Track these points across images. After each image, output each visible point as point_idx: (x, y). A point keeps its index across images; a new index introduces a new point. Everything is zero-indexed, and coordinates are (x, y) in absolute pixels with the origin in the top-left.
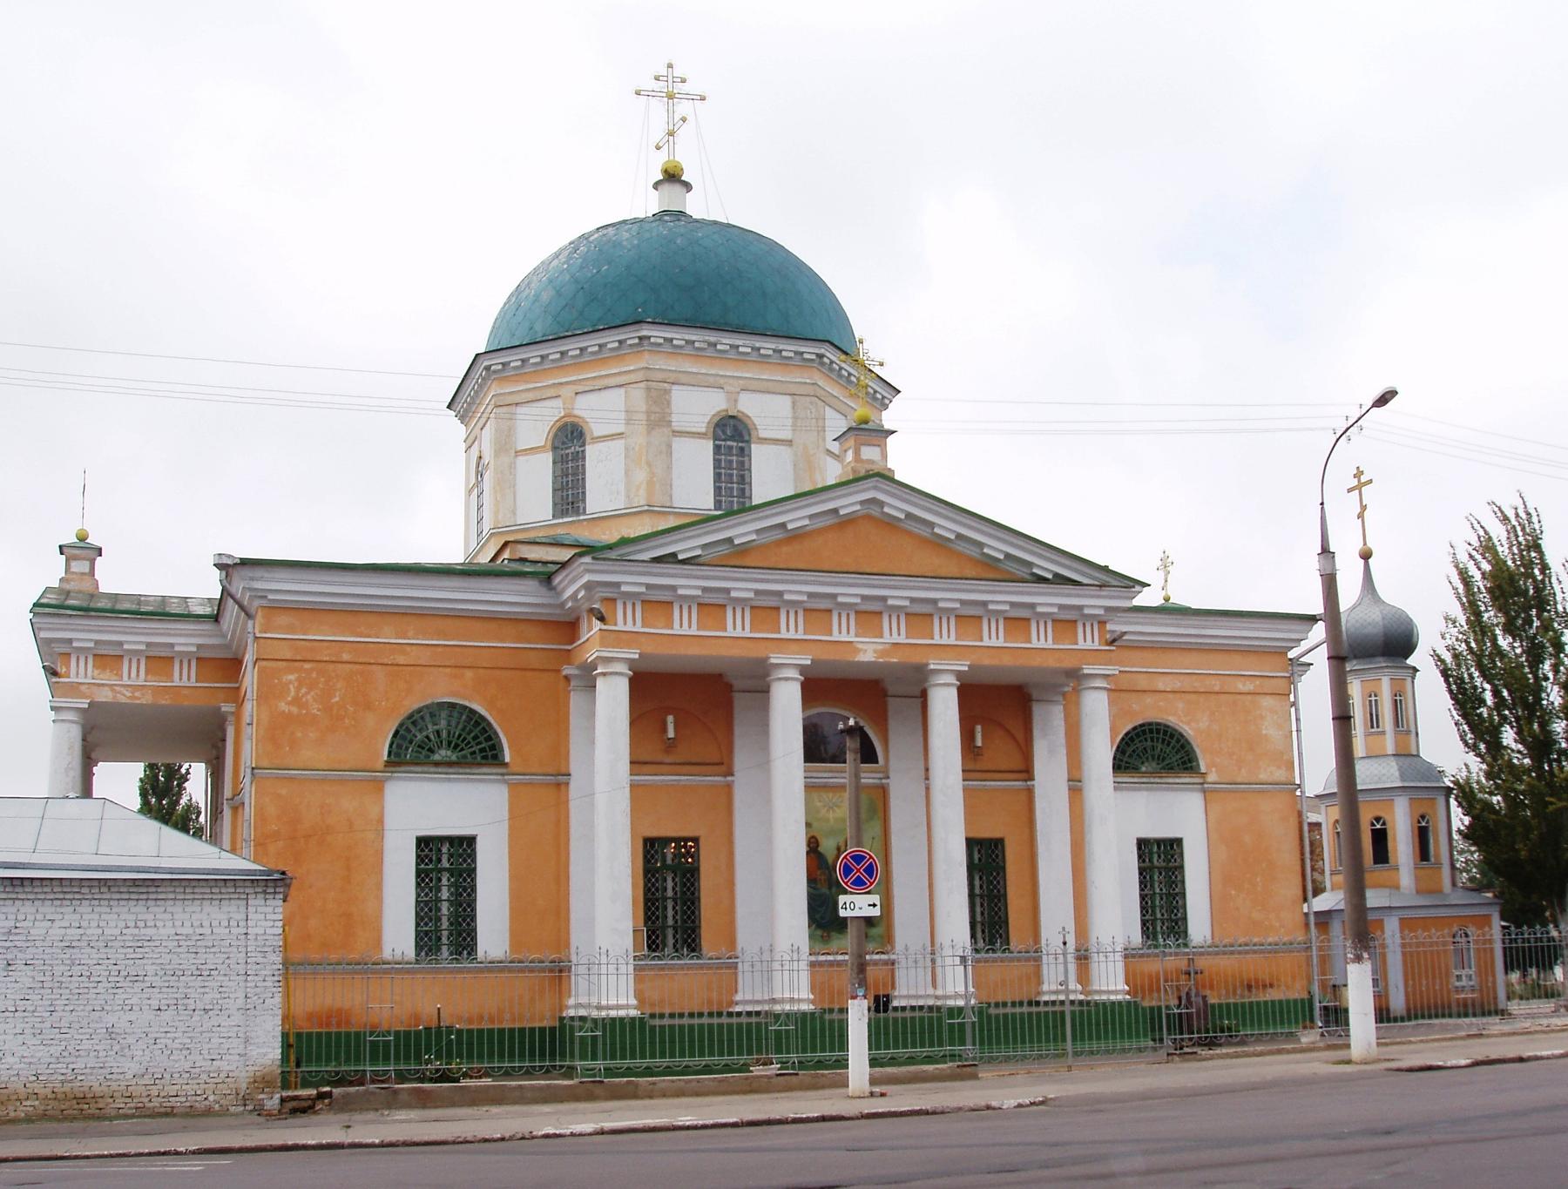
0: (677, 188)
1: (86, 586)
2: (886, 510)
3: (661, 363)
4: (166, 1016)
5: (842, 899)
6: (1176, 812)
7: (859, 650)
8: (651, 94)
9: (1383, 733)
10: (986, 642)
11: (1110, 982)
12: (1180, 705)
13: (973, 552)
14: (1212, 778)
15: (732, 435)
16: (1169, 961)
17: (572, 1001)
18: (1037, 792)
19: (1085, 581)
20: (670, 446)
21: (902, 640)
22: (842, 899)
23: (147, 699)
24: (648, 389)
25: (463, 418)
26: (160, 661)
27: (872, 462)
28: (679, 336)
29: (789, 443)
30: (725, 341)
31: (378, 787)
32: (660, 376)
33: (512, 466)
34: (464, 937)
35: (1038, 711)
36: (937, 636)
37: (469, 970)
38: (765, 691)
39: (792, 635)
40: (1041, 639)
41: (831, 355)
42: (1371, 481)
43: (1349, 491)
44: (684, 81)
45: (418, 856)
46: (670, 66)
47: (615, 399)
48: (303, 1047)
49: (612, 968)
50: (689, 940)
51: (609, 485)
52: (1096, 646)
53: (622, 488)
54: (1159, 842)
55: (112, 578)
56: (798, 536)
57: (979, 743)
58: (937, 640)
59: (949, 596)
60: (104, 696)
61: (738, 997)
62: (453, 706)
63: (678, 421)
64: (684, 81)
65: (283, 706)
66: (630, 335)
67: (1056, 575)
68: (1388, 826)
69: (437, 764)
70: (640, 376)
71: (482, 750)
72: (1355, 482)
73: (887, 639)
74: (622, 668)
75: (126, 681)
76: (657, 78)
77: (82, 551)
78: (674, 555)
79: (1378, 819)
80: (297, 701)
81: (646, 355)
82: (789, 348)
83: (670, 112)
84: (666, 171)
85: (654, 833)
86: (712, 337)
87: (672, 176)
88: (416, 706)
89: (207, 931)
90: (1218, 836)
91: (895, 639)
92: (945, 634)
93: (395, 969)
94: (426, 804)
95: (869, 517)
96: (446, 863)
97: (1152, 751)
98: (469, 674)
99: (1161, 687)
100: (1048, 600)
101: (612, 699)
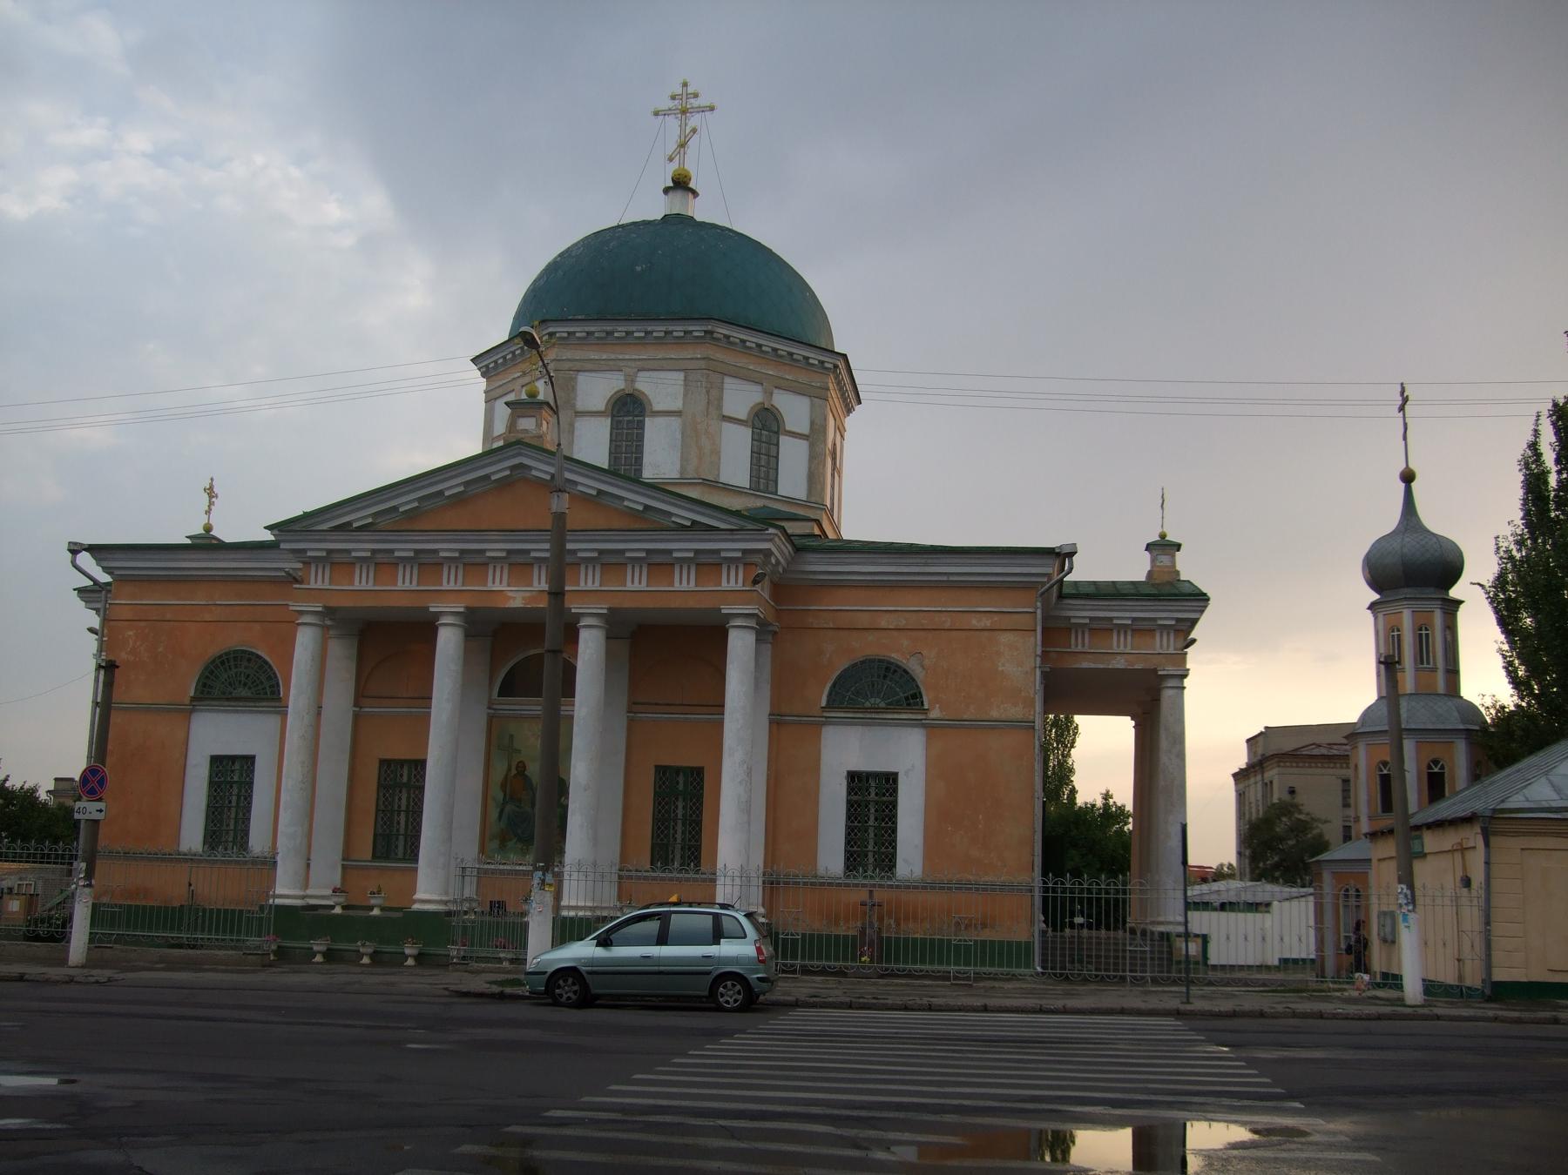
2: (493, 478)
8: (701, 109)
9: (1434, 670)
12: (906, 643)
15: (628, 411)
19: (723, 526)
29: (678, 413)
32: (567, 365)
34: (888, 861)
36: (677, 583)
37: (695, 880)
39: (590, 587)
44: (696, 96)
46: (685, 85)
52: (740, 587)
64: (696, 96)
67: (694, 522)
76: (673, 98)
78: (349, 523)
79: (1436, 762)
83: (683, 126)
87: (681, 184)
90: (937, 769)
92: (450, 581)
93: (190, 859)
94: (217, 733)
99: (884, 624)
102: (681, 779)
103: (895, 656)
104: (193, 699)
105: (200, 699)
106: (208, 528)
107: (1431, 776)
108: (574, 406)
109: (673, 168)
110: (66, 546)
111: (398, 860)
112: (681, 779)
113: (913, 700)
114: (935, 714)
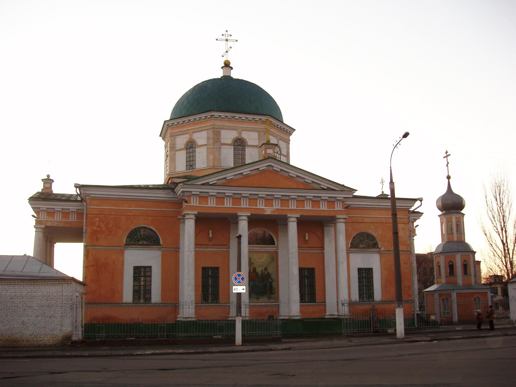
0: (228, 68)
1: (48, 191)
3: (218, 123)
4: (39, 318)
5: (234, 287)
6: (373, 261)
7: (266, 211)
8: (221, 40)
10: (306, 208)
11: (188, 311)
12: (372, 227)
13: (302, 181)
14: (382, 249)
15: (239, 144)
16: (366, 306)
17: (179, 316)
18: (326, 254)
20: (220, 148)
21: (279, 207)
22: (234, 287)
23: (62, 225)
24: (214, 131)
25: (164, 139)
26: (66, 214)
27: (270, 154)
28: (223, 115)
29: (206, 145)
30: (237, 116)
31: (122, 253)
33: (175, 155)
34: (148, 299)
35: (326, 229)
38: (237, 223)
40: (323, 207)
41: (271, 119)
42: (450, 155)
43: (444, 157)
44: (231, 36)
45: (134, 272)
46: (227, 31)
47: (204, 134)
48: (90, 328)
49: (187, 306)
50: (216, 298)
51: (202, 160)
52: (341, 209)
53: (206, 161)
54: (365, 269)
55: (57, 189)
56: (247, 176)
57: (307, 239)
58: (290, 208)
59: (293, 194)
60: (50, 224)
61: (230, 315)
62: (145, 228)
63: (223, 141)
64: (231, 36)
65: (95, 228)
66: (208, 114)
67: (328, 187)
68: (454, 264)
69: (140, 245)
70: (211, 127)
71: (154, 241)
72: (446, 155)
73: (275, 207)
74: (193, 217)
75: (56, 219)
76: (223, 35)
77: (48, 181)
78: (208, 183)
79: (451, 261)
80: (98, 226)
81: (213, 121)
82: (257, 117)
84: (225, 64)
85: (206, 266)
86: (233, 115)
87: (227, 65)
88: (134, 228)
89: (51, 294)
91: (277, 207)
93: (127, 305)
94: (135, 257)
95: (269, 170)
96: (142, 273)
97: (362, 242)
98: (150, 218)
99: (366, 221)
100: (325, 195)
101: (189, 227)
102: (306, 271)
103: (370, 231)
104: (125, 245)
105: (128, 245)
106: (383, 192)
107: (450, 265)
108: (220, 141)
109: (224, 59)
110: (74, 185)
111: (307, 302)
112: (306, 271)
113: (375, 245)
114: (382, 249)
